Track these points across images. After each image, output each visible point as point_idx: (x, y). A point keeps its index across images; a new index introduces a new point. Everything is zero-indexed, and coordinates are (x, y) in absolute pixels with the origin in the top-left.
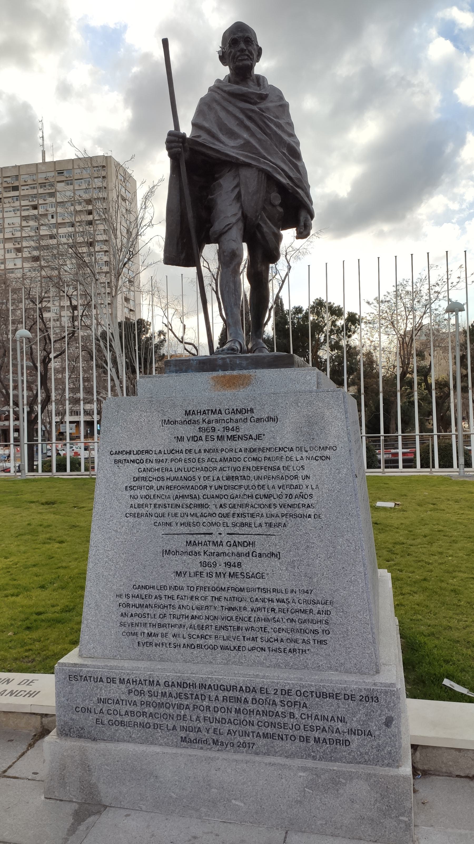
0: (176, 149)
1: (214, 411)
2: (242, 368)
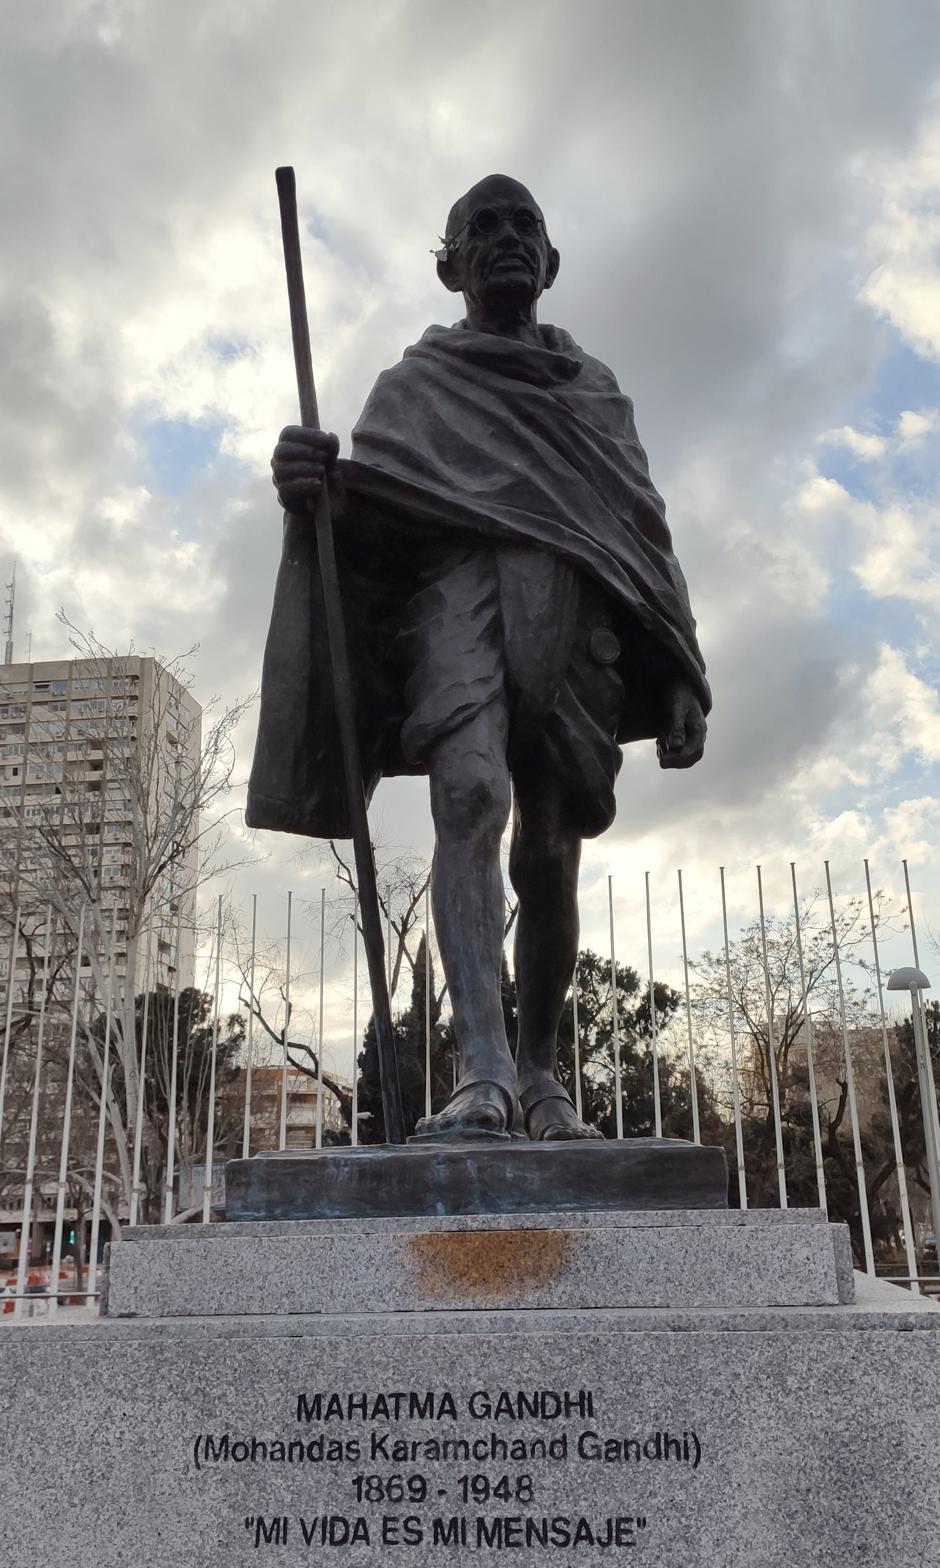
0: (309, 480)
1: (422, 1399)
2: (523, 1199)
